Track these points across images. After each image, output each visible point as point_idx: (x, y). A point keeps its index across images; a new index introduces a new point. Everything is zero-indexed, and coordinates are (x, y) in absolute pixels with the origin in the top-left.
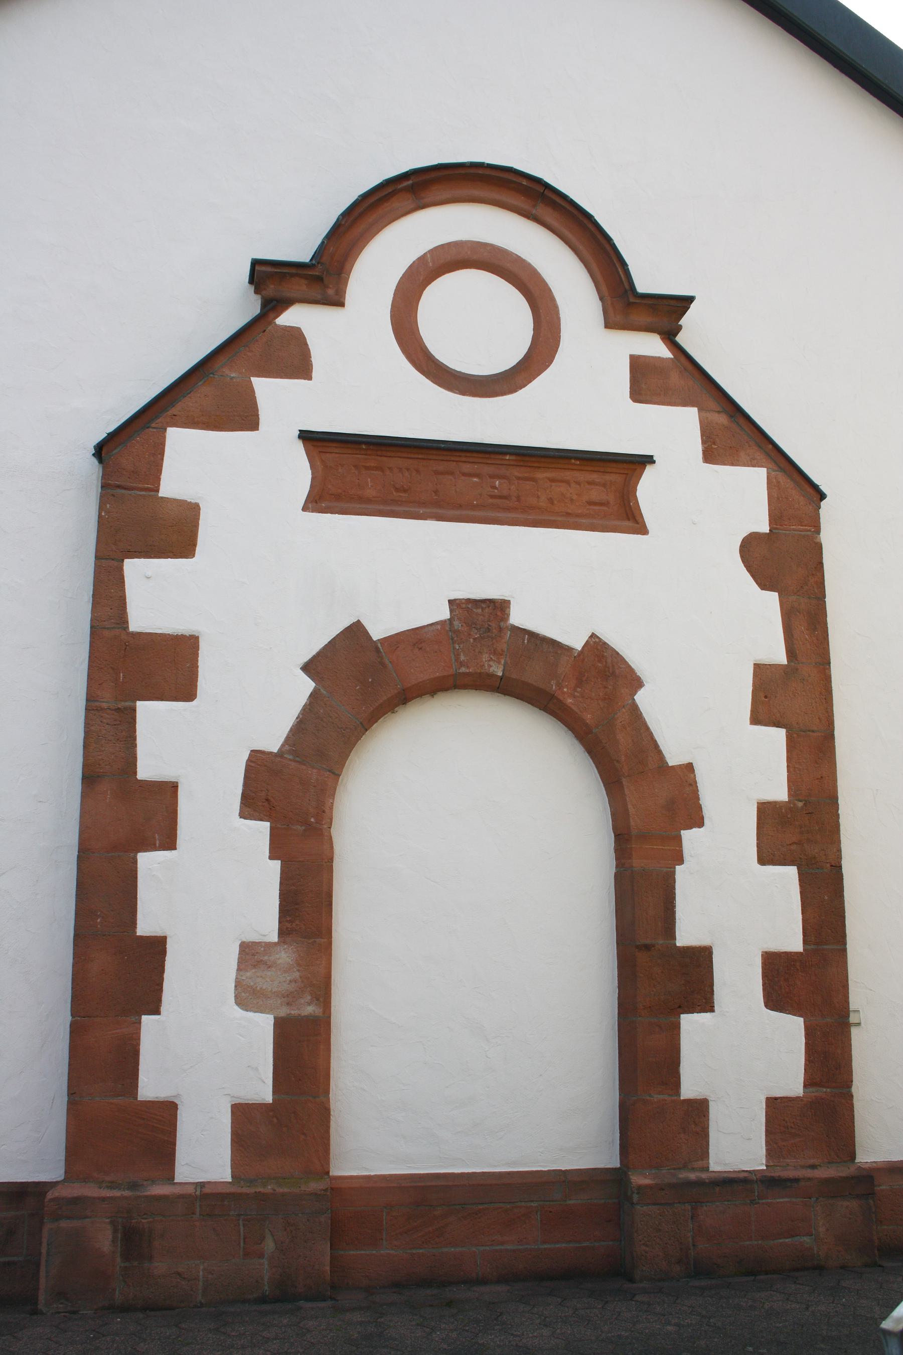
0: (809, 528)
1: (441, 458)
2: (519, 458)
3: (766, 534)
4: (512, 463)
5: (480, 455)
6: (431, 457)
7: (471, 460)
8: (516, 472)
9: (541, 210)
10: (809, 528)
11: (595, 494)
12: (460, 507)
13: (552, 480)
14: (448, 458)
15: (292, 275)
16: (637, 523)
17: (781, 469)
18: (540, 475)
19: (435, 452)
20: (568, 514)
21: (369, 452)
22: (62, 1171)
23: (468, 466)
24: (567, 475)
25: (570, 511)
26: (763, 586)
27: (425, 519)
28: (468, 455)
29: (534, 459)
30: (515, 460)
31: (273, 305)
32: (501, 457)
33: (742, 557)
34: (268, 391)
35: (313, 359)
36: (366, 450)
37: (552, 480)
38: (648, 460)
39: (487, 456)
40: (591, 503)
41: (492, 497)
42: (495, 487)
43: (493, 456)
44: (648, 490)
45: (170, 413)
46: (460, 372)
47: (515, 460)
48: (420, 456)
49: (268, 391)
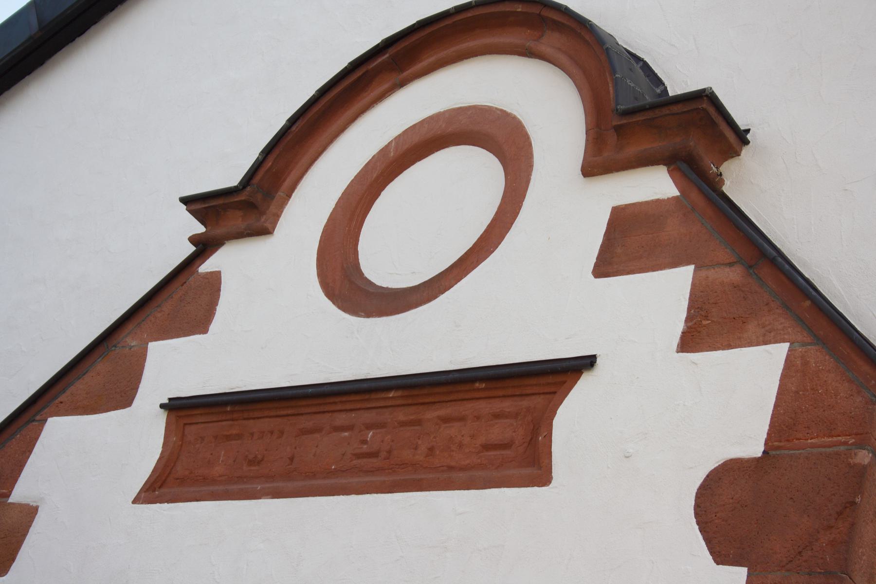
0: (842, 439)
1: (314, 409)
2: (406, 393)
3: (757, 460)
4: (399, 402)
5: (358, 397)
6: (303, 410)
7: (348, 406)
8: (401, 415)
9: (550, 41)
10: (842, 439)
11: (497, 432)
12: (314, 476)
13: (446, 420)
14: (322, 409)
15: (226, 207)
16: (540, 468)
17: (819, 340)
18: (431, 414)
19: (304, 403)
20: (451, 468)
21: (235, 415)
22: (761, 449)
23: (343, 416)
24: (467, 408)
25: (453, 464)
26: (721, 557)
27: (260, 498)
28: (344, 399)
29: (425, 391)
30: (402, 397)
31: (204, 247)
32: (383, 395)
33: (697, 507)
34: (668, 291)
35: (218, 308)
36: (232, 412)
37: (446, 420)
38: (571, 370)
39: (367, 397)
40: (487, 447)
41: (359, 456)
42: (364, 442)
43: (374, 396)
44: (575, 419)
45: (59, 399)
46: (387, 288)
47: (402, 397)
48: (289, 412)
49: (668, 291)
